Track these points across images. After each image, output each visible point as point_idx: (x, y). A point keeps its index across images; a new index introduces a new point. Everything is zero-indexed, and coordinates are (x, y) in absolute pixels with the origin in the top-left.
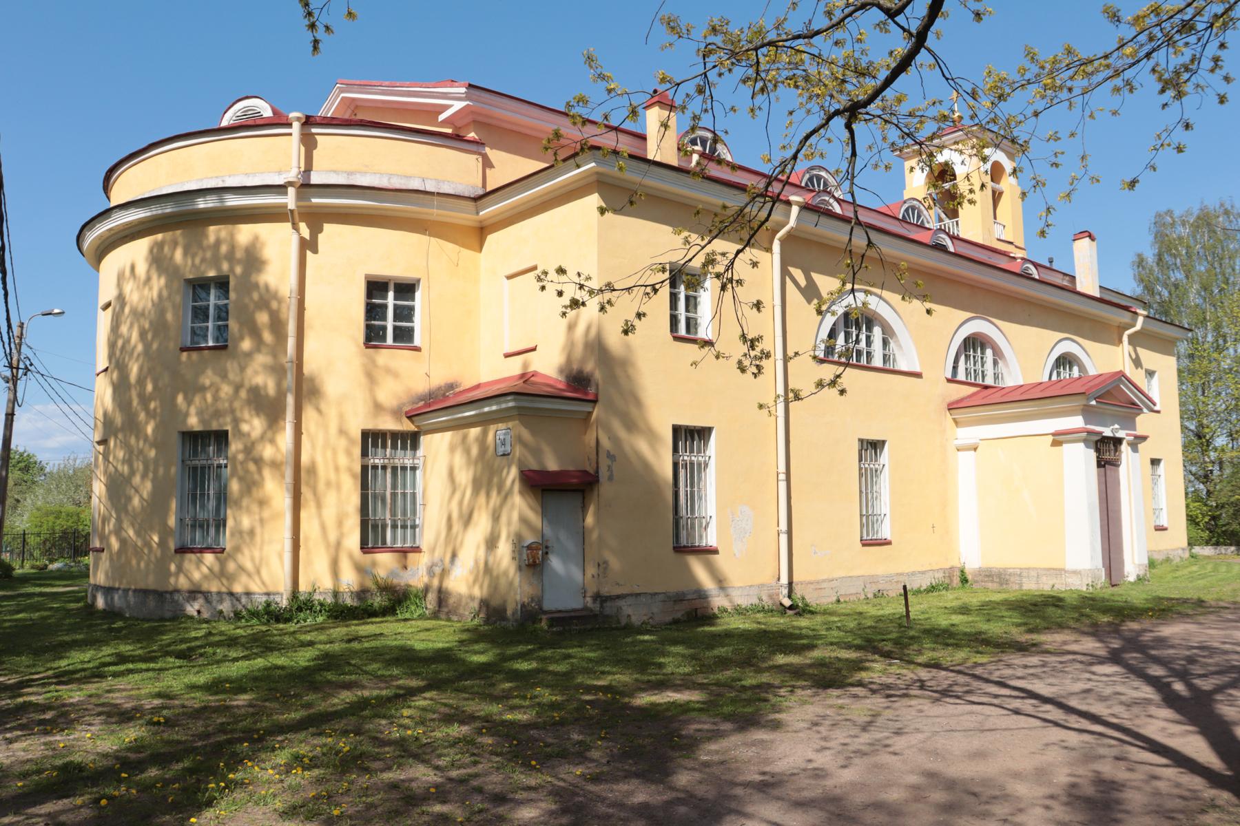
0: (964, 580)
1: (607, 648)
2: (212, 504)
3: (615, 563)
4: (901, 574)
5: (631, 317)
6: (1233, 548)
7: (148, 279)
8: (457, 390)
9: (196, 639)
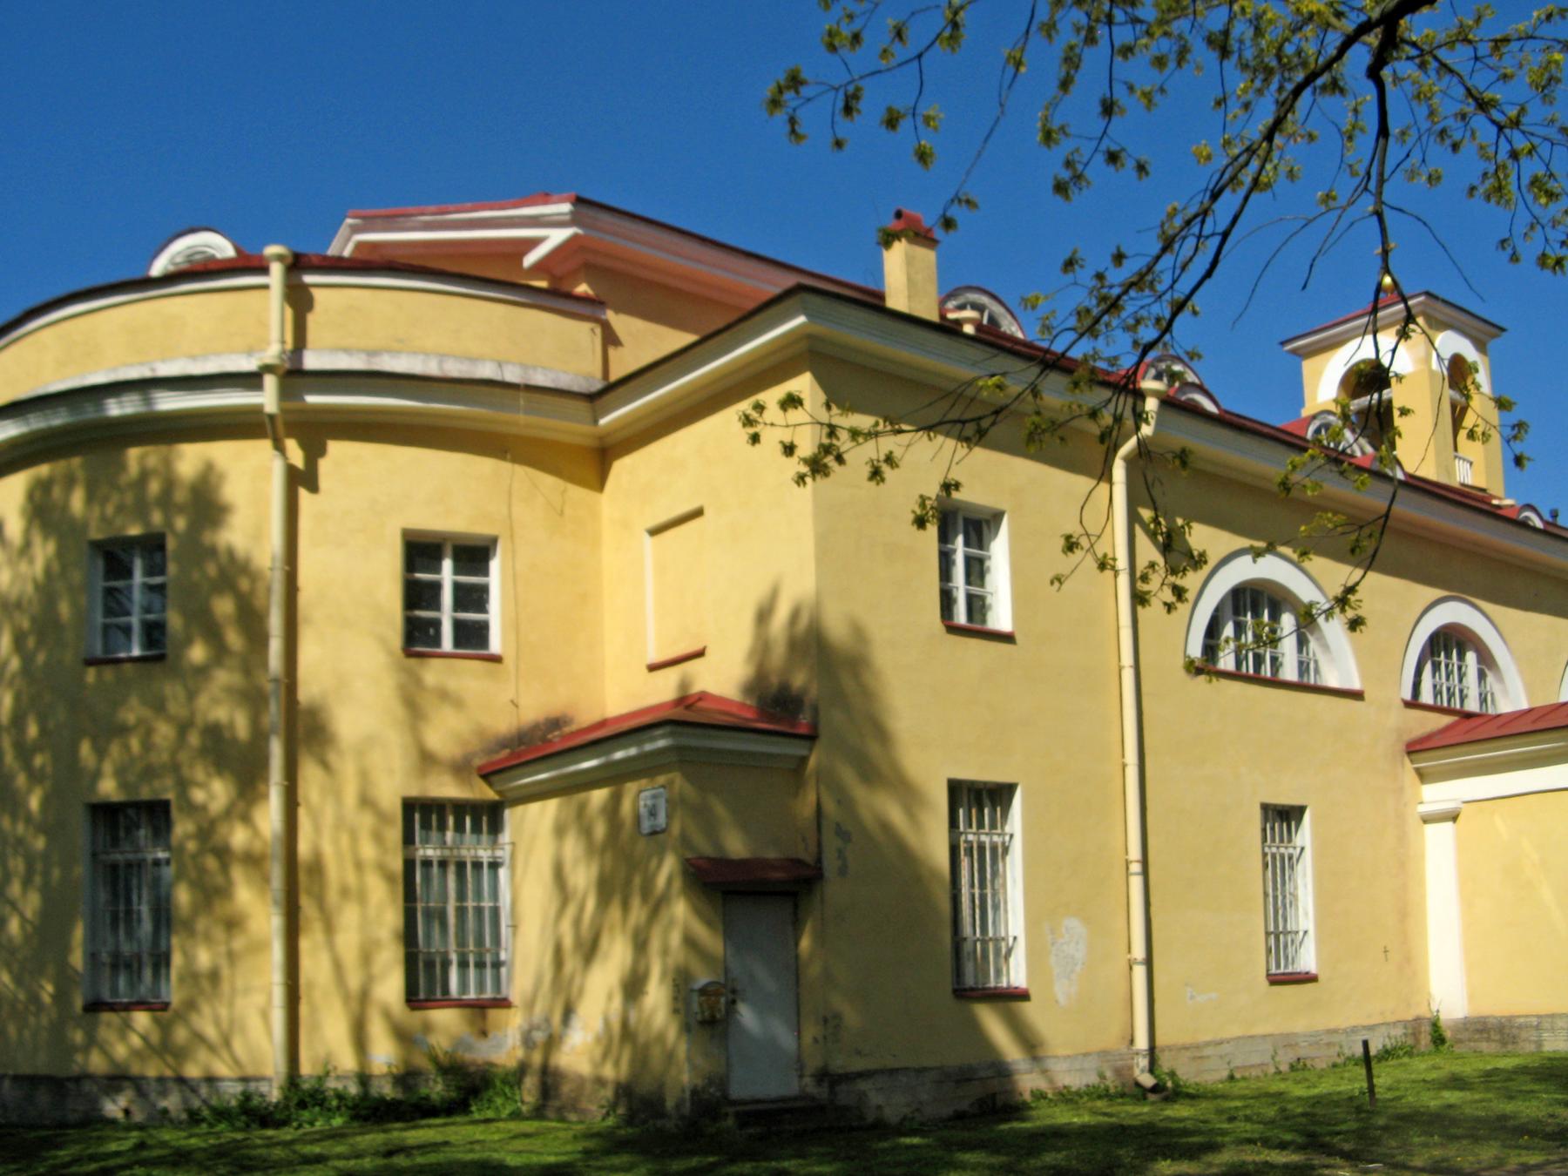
0: (1438, 1040)
1: (852, 1159)
2: (147, 926)
3: (852, 1018)
4: (1335, 1031)
7: (27, 546)
8: (567, 730)
9: (117, 1154)
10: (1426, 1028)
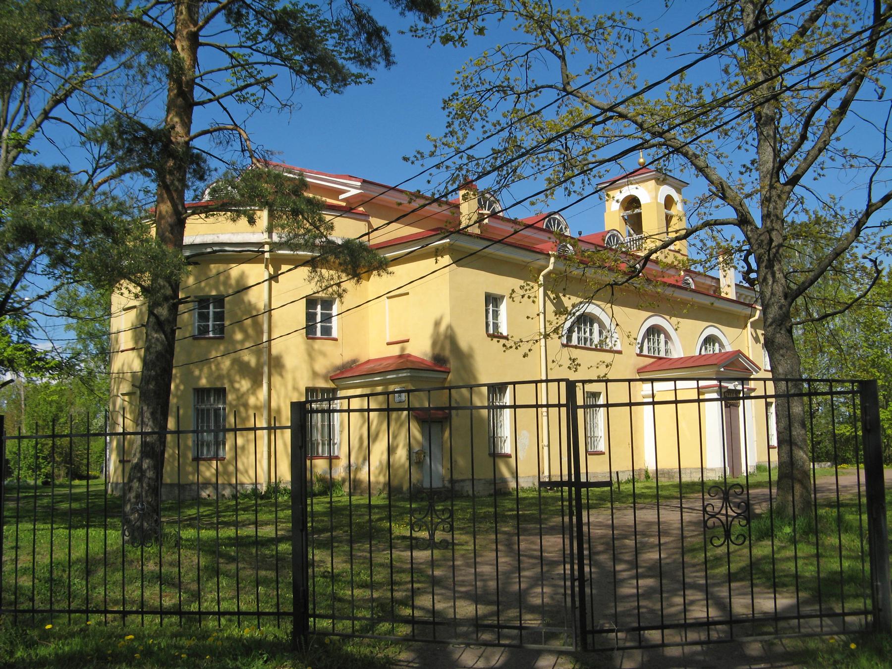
5: (527, 351)
6: (829, 463)
10: (644, 473)
